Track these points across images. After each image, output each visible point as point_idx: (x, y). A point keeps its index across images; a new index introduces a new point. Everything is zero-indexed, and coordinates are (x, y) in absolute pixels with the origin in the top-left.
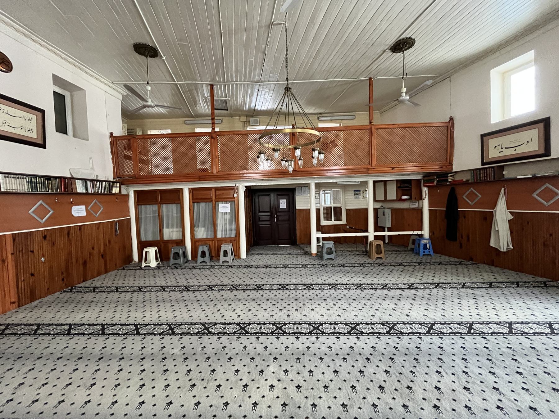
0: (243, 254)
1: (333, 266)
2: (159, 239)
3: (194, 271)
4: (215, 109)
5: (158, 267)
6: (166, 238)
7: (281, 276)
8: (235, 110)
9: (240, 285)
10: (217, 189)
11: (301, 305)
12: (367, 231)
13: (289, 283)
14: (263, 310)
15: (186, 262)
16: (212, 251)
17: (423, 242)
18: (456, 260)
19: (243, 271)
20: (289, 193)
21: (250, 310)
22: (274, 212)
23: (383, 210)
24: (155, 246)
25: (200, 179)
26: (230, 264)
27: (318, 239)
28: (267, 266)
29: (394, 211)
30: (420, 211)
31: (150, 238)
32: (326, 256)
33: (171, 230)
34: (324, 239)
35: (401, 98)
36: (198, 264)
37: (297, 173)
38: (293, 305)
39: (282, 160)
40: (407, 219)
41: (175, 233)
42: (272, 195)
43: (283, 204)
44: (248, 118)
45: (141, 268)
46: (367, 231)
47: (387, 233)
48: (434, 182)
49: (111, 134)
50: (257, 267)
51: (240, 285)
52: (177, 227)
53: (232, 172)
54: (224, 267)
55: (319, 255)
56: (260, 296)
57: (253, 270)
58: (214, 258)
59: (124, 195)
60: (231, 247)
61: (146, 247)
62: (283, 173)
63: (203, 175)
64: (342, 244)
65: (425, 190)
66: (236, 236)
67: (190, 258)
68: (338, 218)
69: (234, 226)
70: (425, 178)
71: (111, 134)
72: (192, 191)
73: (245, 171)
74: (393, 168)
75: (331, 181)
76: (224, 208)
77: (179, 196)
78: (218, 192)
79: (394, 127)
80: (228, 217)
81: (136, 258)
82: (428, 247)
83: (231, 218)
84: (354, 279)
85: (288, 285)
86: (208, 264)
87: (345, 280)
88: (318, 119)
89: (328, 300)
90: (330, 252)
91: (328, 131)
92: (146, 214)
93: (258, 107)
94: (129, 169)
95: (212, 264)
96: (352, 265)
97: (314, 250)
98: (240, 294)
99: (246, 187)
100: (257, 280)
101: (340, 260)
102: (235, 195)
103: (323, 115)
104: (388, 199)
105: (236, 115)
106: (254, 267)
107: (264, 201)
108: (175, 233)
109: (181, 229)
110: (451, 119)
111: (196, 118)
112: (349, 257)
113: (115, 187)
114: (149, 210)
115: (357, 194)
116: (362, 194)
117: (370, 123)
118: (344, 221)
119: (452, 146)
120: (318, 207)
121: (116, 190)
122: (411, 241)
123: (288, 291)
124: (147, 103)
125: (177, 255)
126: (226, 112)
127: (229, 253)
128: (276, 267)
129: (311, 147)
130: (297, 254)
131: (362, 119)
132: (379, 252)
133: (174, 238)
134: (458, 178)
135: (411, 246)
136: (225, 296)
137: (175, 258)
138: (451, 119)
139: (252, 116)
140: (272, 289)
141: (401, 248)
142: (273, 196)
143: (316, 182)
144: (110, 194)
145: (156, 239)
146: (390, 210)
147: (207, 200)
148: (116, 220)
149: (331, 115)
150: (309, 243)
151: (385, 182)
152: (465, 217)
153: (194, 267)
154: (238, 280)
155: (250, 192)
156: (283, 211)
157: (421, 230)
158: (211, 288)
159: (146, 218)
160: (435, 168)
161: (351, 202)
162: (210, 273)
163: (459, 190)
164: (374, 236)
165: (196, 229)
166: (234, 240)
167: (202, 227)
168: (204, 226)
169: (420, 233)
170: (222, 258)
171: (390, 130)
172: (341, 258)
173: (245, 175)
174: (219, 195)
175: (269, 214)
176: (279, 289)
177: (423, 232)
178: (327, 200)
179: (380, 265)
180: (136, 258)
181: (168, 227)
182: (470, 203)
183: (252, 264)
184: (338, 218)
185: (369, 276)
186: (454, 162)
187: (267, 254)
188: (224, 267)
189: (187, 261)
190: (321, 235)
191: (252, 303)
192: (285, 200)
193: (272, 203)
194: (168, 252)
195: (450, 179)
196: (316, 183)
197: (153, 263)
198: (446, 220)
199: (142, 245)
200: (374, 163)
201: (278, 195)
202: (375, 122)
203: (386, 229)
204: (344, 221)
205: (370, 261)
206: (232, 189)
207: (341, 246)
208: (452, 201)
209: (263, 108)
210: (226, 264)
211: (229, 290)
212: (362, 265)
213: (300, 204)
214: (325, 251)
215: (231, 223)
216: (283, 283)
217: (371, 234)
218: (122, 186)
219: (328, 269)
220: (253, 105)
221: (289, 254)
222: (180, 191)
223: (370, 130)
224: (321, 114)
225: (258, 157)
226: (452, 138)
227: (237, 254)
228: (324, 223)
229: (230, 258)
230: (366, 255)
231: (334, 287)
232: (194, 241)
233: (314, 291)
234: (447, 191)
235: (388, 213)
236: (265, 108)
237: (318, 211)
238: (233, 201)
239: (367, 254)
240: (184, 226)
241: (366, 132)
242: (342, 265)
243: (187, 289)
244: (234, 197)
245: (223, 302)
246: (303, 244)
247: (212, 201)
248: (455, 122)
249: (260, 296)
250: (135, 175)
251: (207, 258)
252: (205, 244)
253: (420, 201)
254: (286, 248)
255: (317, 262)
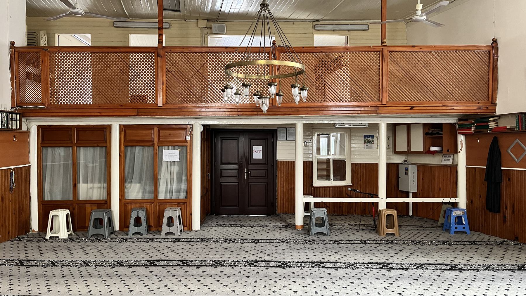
0: (196, 224)
1: (323, 242)
2: (71, 198)
3: (126, 244)
4: (165, 9)
5: (70, 239)
6: (82, 196)
7: (249, 252)
8: (190, 12)
9: (192, 261)
10: (161, 127)
11: (271, 282)
12: (377, 196)
13: (258, 259)
14: (222, 285)
15: (112, 233)
16: (151, 218)
17: (456, 213)
18: (499, 240)
19: (195, 246)
20: (268, 136)
21: (206, 285)
22: (244, 164)
23: (406, 166)
24: (66, 208)
25: (139, 113)
26: (176, 236)
27: (307, 206)
28: (230, 241)
29: (422, 169)
30: (454, 169)
31: (58, 197)
32: (315, 230)
33: (90, 185)
34: (317, 205)
35: (415, 18)
36: (130, 235)
37: (274, 110)
38: (263, 282)
39: (255, 95)
40: (437, 180)
41: (95, 190)
42: (242, 139)
43: (257, 152)
44: (209, 23)
45: (46, 240)
46: (377, 196)
47: (411, 200)
48: (471, 128)
49: (12, 43)
50: (216, 241)
51: (192, 261)
52: (100, 182)
53: (185, 105)
54: (169, 240)
55: (306, 229)
56: (219, 273)
57: (211, 245)
58: (153, 229)
59: (24, 132)
60: (178, 212)
61: (53, 209)
62: (256, 110)
63: (140, 107)
64: (344, 215)
65: (461, 138)
66: (186, 197)
67: (117, 228)
68: (340, 174)
69: (183, 186)
70: (461, 123)
71: (12, 43)
72: (124, 129)
73: (204, 105)
74: (412, 108)
75: (326, 122)
76: (170, 155)
77: (105, 136)
78: (163, 133)
79: (413, 50)
80: (176, 169)
81: (35, 226)
82: (464, 222)
83: (181, 172)
84: (348, 257)
85: (257, 262)
86: (145, 236)
87: (334, 258)
88: (314, 27)
89: (307, 278)
90: (321, 223)
91: (322, 52)
92: (53, 161)
93: (226, 9)
94: (33, 93)
95: (151, 236)
96: (350, 242)
97: (299, 221)
98: (192, 270)
99: (204, 126)
100: (216, 256)
101: (336, 235)
102: (188, 138)
103: (321, 23)
104: (412, 150)
105: (191, 18)
106: (212, 240)
107: (230, 148)
108: (95, 190)
109: (105, 185)
110: (495, 41)
111: (132, 20)
112: (349, 233)
113: (14, 120)
114: (59, 155)
115: (369, 142)
116: (375, 142)
117: (382, 43)
118: (348, 182)
119: (495, 79)
120: (310, 159)
121: (14, 125)
122: (442, 212)
123: (256, 268)
124: (76, 11)
125: (99, 222)
126: (178, 13)
127: (176, 221)
128: (243, 241)
129: (292, 81)
130: (275, 227)
131: (371, 38)
132: (390, 226)
133: (94, 198)
134: (502, 124)
135: (441, 220)
136: (174, 272)
137: (95, 227)
138: (495, 41)
139: (216, 20)
140: (236, 266)
141: (424, 222)
142: (243, 140)
143: (305, 122)
144: (8, 130)
145: (66, 199)
146: (415, 167)
147: (149, 143)
148: (12, 167)
149: (334, 24)
150: (292, 212)
151: (409, 125)
152: (509, 180)
153: (126, 240)
154: (190, 255)
155: (210, 134)
156: (257, 162)
157: (456, 196)
158: (118, 263)
159: (52, 166)
160: (472, 109)
161: (358, 153)
162: (149, 247)
163: (503, 141)
164: (387, 203)
165: (127, 185)
166: (184, 203)
167: (135, 183)
168: (140, 181)
169: (453, 200)
170: (165, 229)
171: (408, 55)
172: (337, 233)
173: (203, 110)
174: (165, 136)
175: (236, 166)
176: (245, 266)
177: (458, 200)
178: (328, 148)
179: (389, 242)
180: (35, 226)
181: (86, 181)
182: (516, 159)
183: (209, 237)
184: (340, 174)
185: (369, 254)
186: (498, 102)
187: (230, 226)
188: (169, 240)
189: (113, 232)
190: (312, 200)
191: (209, 279)
192: (260, 147)
193: (242, 150)
194: (86, 219)
195: (491, 125)
196: (304, 125)
197: (63, 234)
198: (486, 183)
199: (46, 207)
200: (386, 99)
201: (251, 139)
202: (388, 42)
203: (411, 195)
204: (348, 182)
205: (377, 237)
206: (184, 128)
207: (343, 217)
208: (495, 157)
209: (232, 11)
210: (170, 236)
211: (177, 265)
212: (364, 242)
213: (281, 156)
214: (314, 221)
215: (179, 181)
216: (251, 260)
217: (382, 200)
218: (23, 119)
219: (314, 246)
220: (217, 7)
221: (264, 226)
222: (109, 128)
223: (381, 53)
224: (318, 20)
225: (223, 91)
226: (495, 68)
227: (187, 224)
228: (317, 183)
229: (177, 228)
230: (374, 230)
231: (318, 265)
232: (124, 203)
233: (290, 269)
234: (487, 142)
235: (413, 171)
236: (236, 11)
237: (308, 166)
238: (185, 148)
239: (376, 229)
240: (109, 180)
241: (375, 56)
242: (337, 242)
243: (120, 264)
244: (186, 141)
245: (171, 278)
246: (285, 214)
247: (153, 145)
248: (499, 46)
249: (219, 273)
250: (42, 104)
251: (143, 229)
252: (141, 208)
253: (455, 155)
254: (262, 219)
255: (302, 237)
